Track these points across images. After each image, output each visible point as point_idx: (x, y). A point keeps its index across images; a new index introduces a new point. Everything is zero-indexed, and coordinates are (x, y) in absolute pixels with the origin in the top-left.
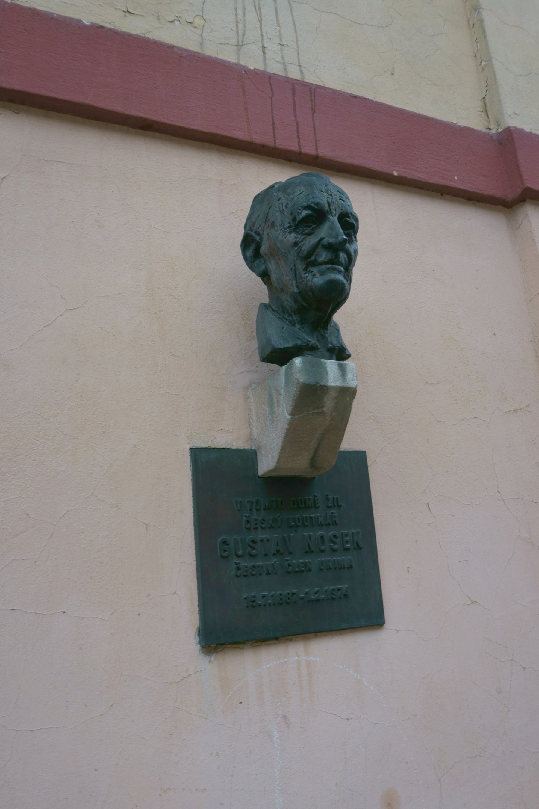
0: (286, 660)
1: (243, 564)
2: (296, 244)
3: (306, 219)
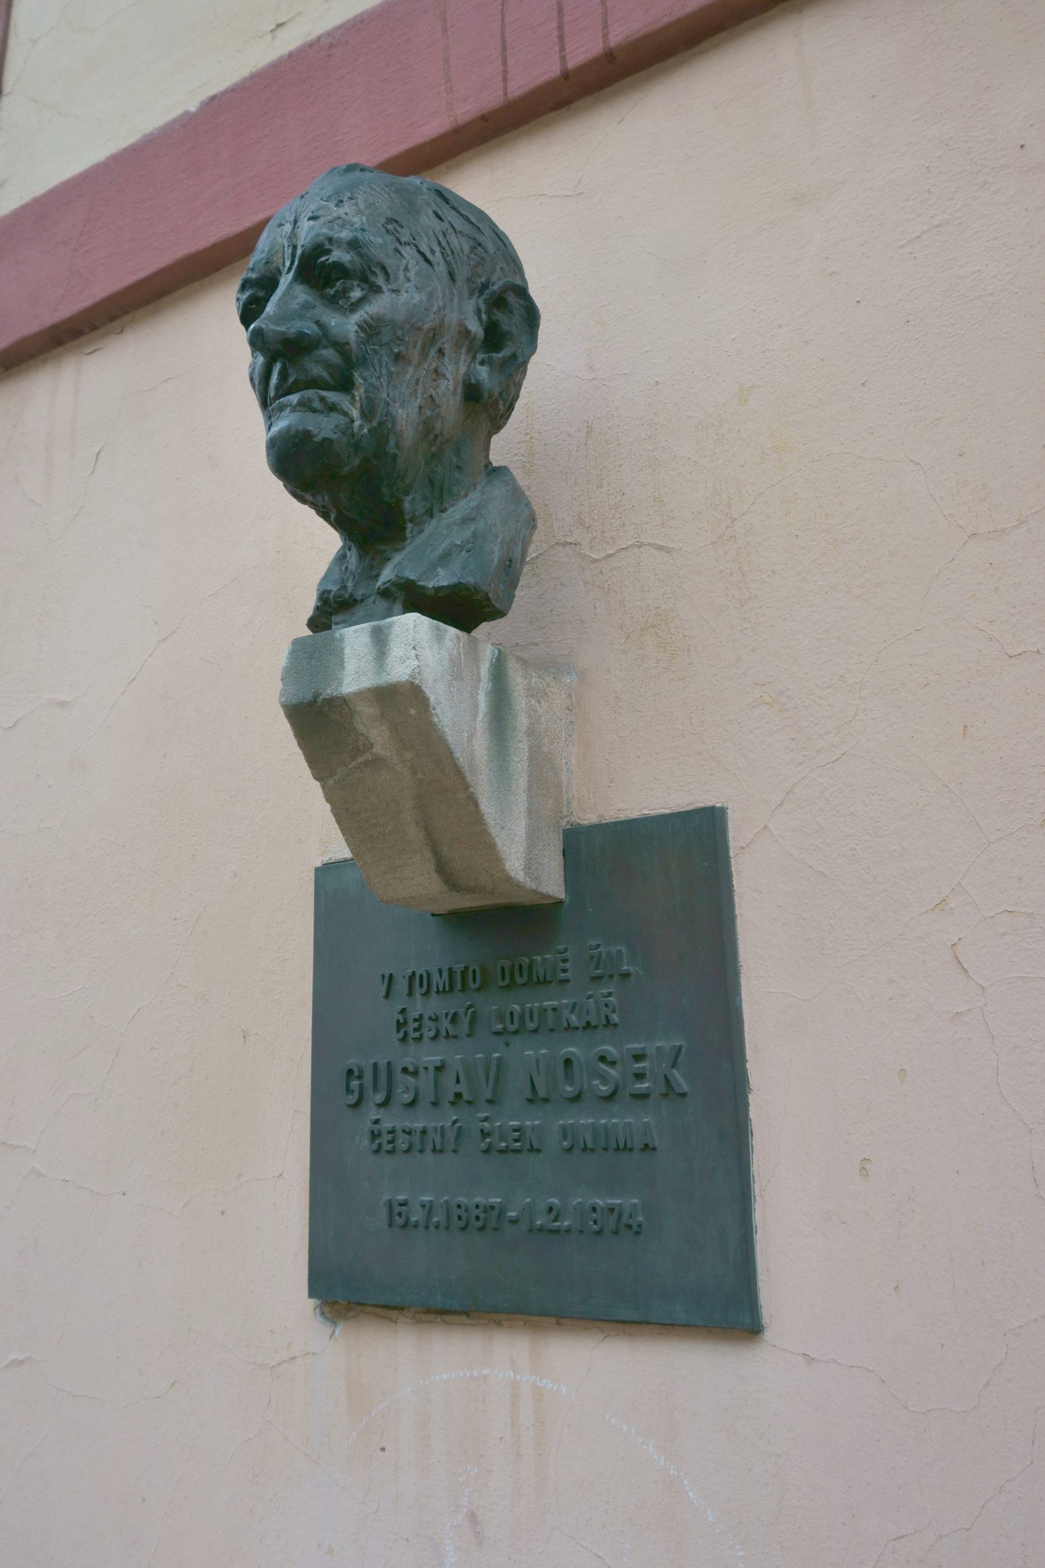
0: (485, 1372)
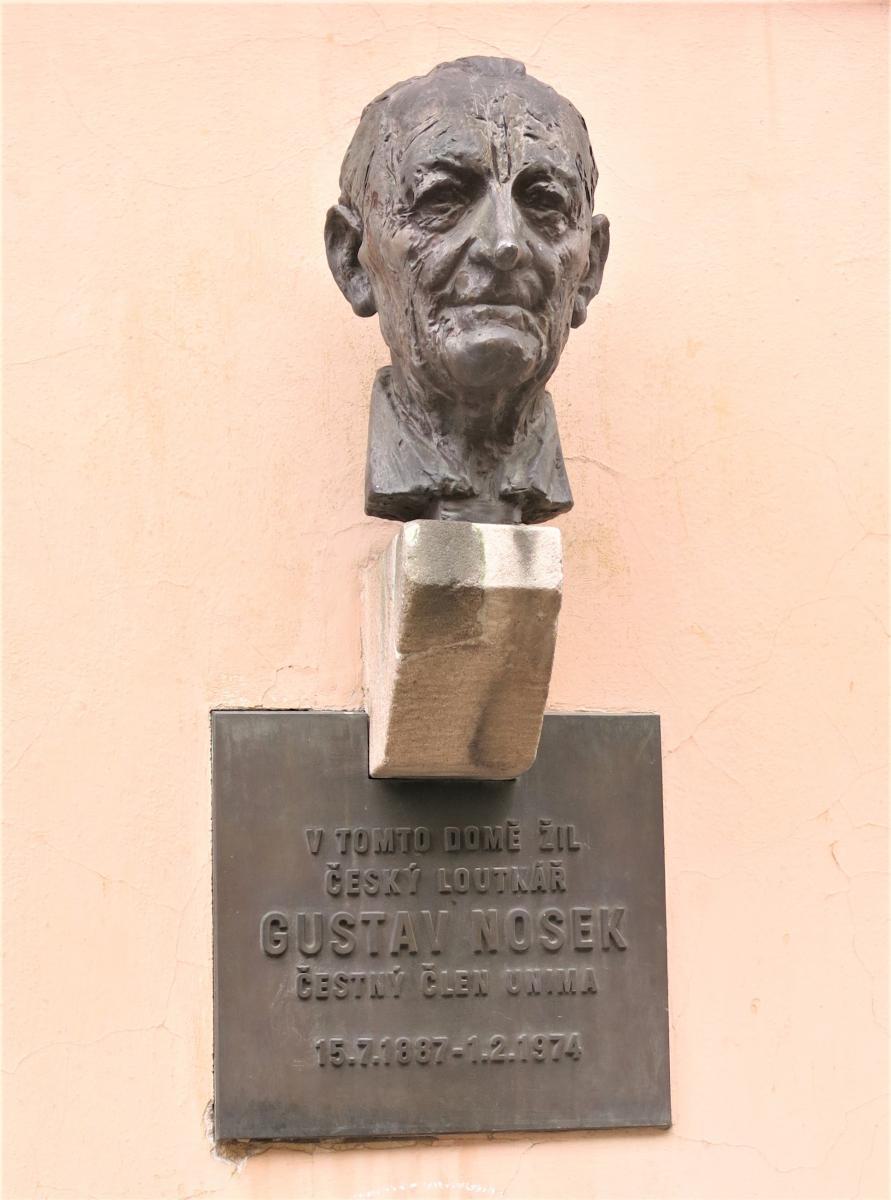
0: (414, 1185)
1: (318, 971)
2: (412, 253)
3: (435, 194)
